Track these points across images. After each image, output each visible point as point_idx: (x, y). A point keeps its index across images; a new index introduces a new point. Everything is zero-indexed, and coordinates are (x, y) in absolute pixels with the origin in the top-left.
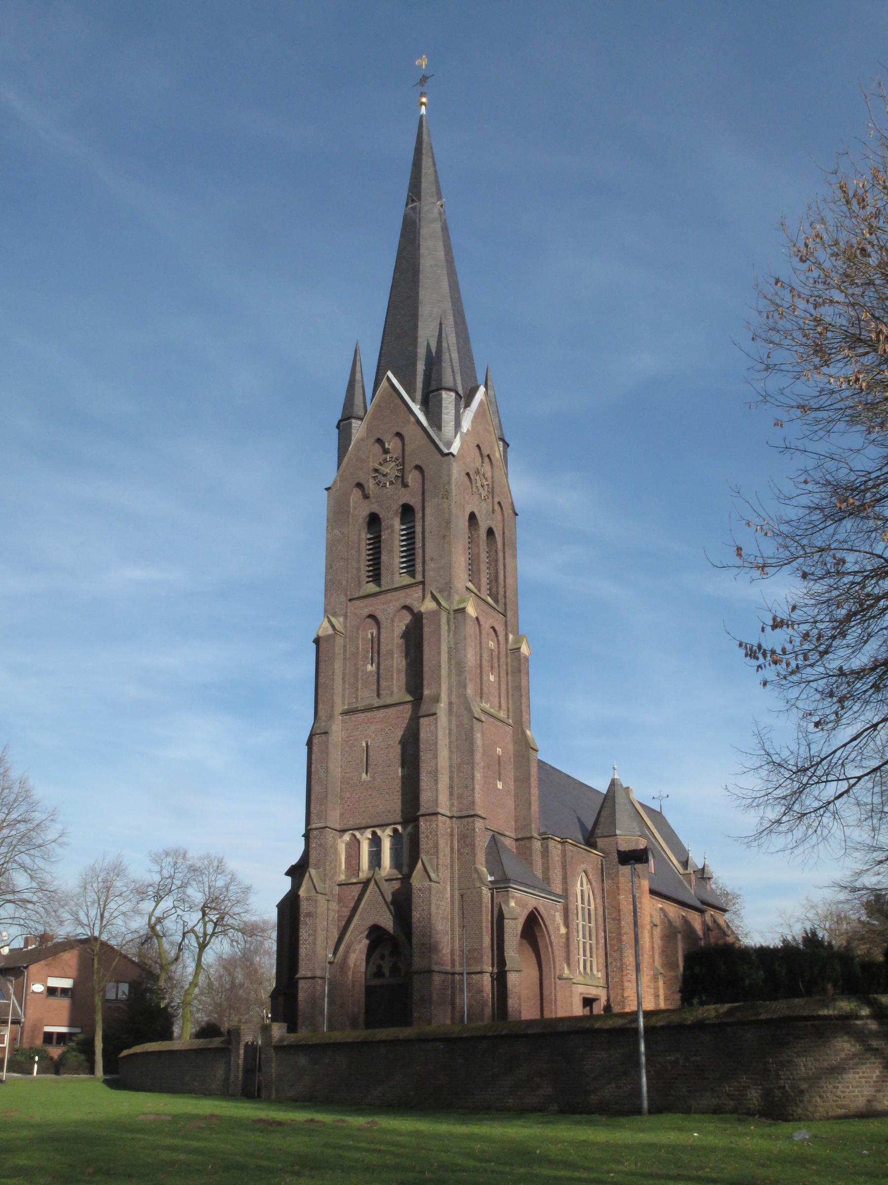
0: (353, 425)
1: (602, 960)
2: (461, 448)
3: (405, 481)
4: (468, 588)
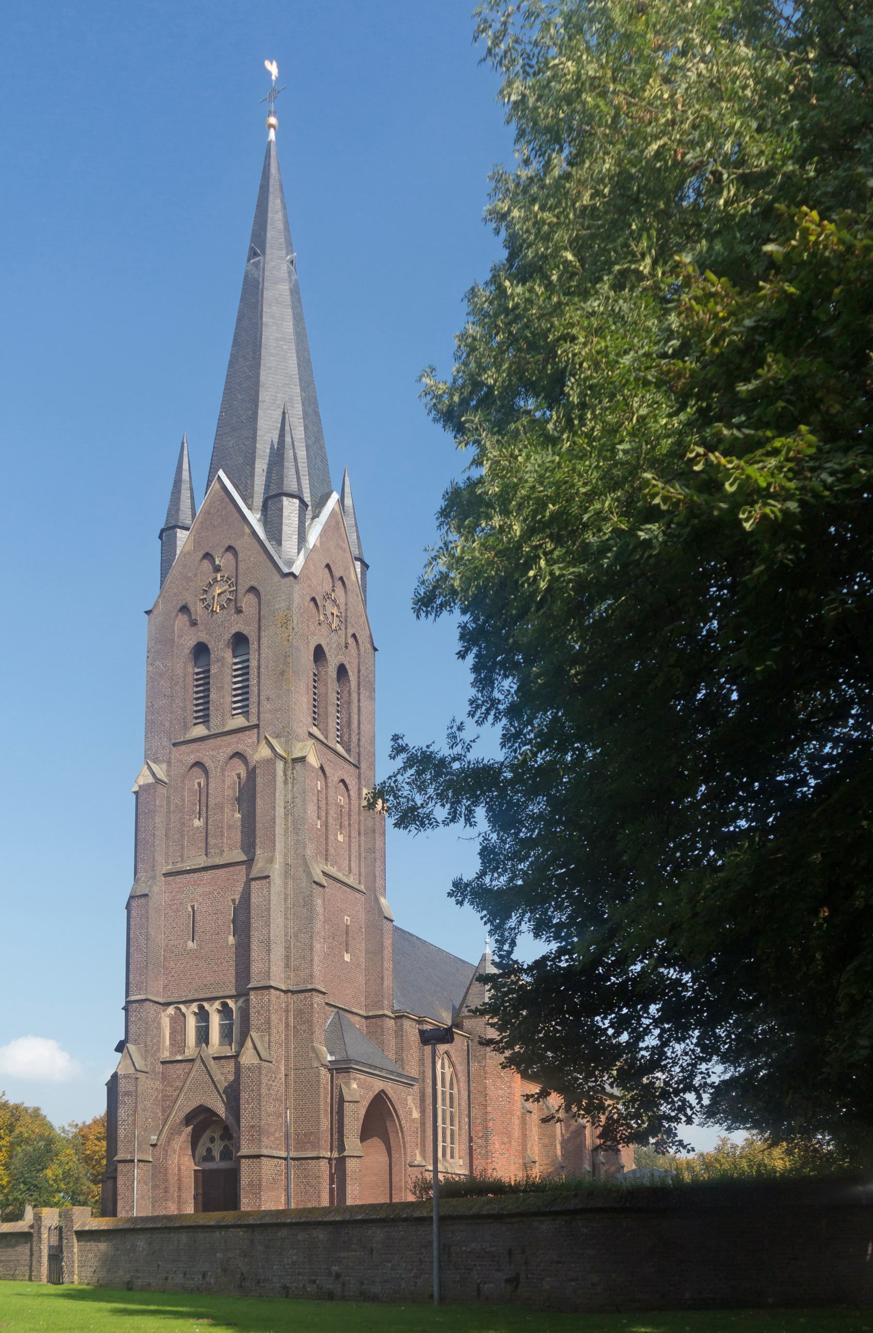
0: (178, 535)
1: (465, 1146)
2: (305, 567)
3: (239, 605)
4: (310, 734)
